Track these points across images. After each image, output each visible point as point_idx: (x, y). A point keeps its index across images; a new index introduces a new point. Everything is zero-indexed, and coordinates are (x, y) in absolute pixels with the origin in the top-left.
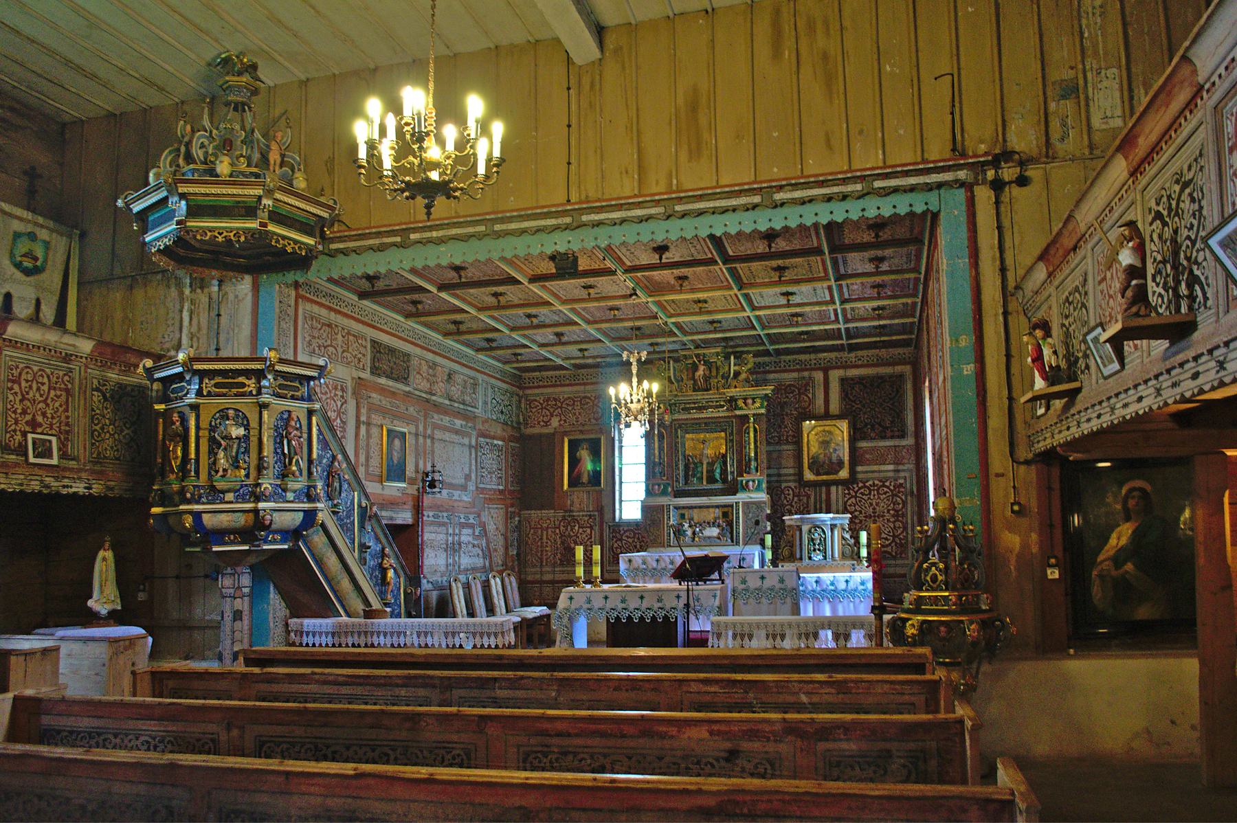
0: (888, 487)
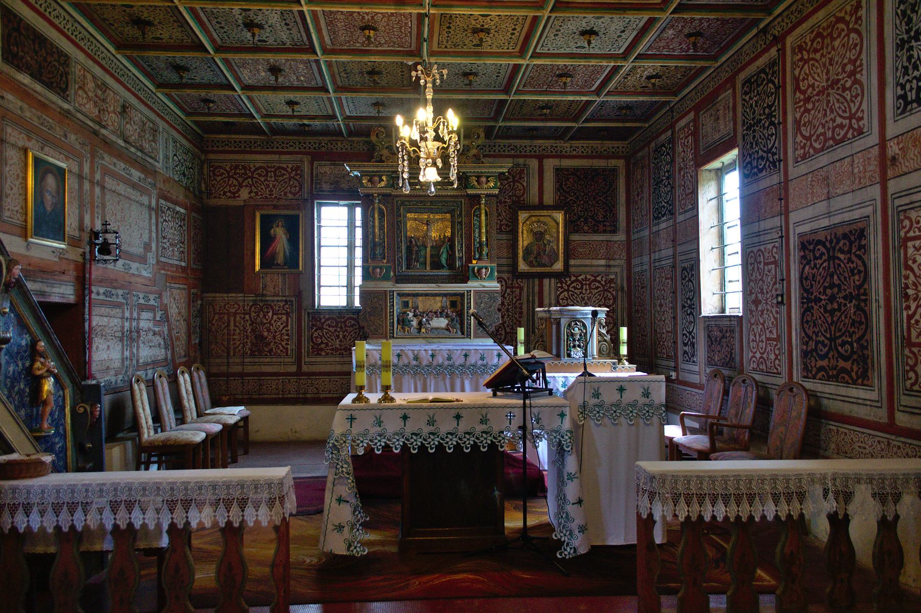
0: (599, 282)
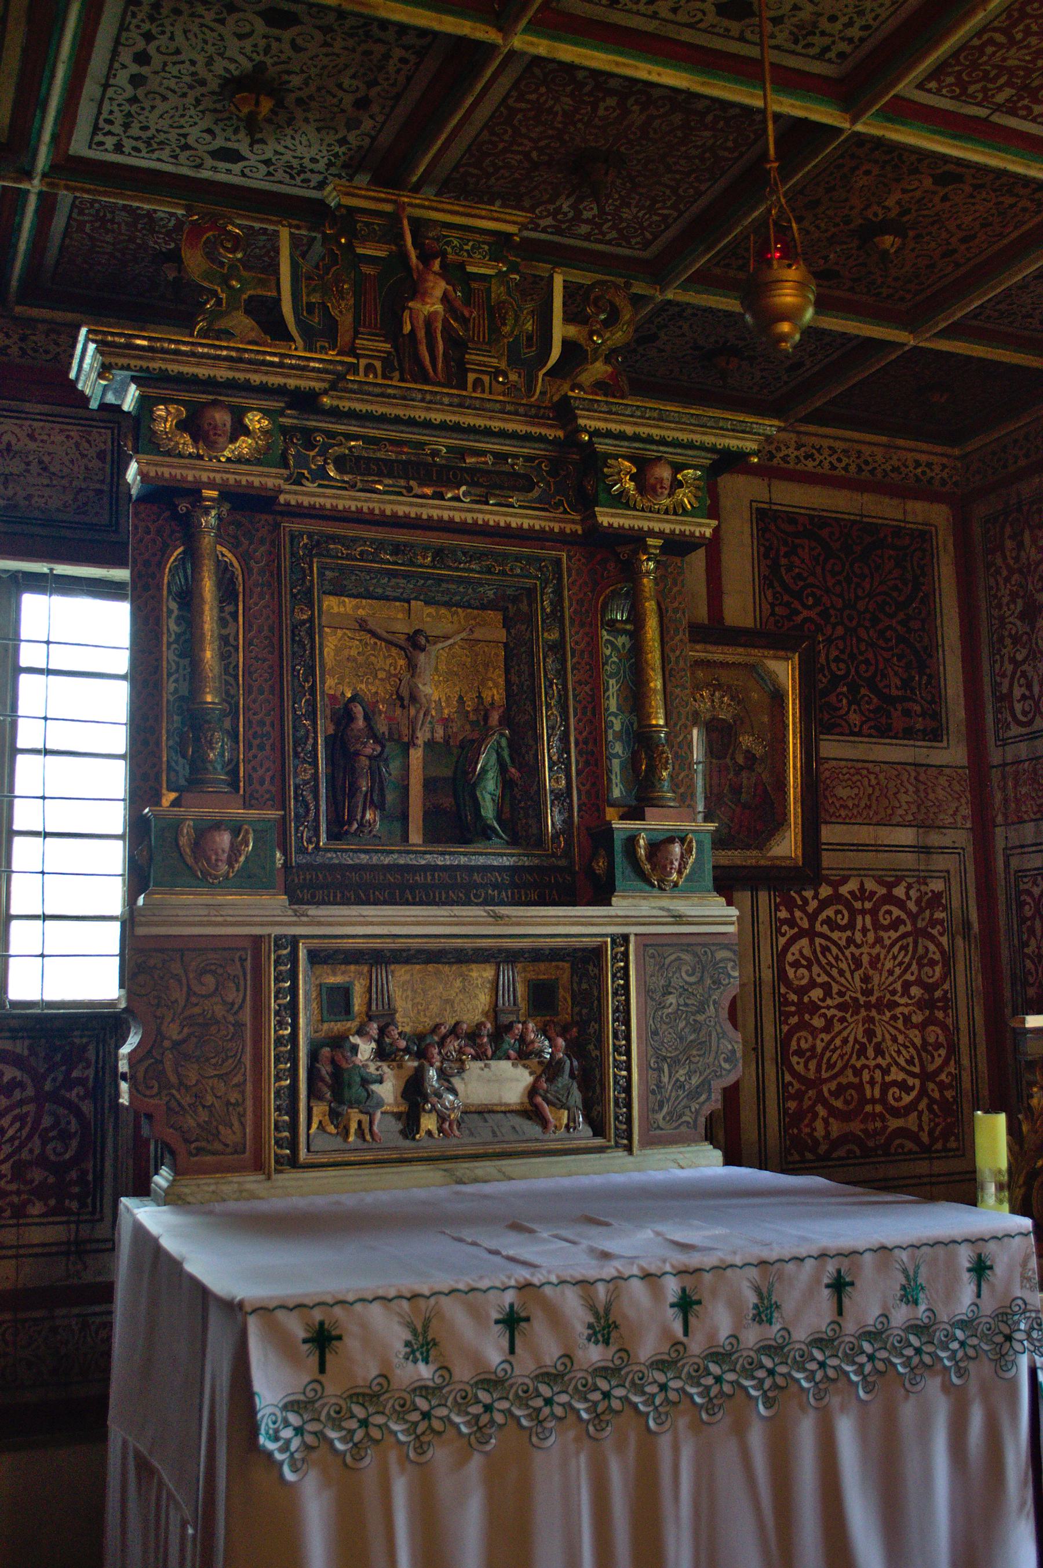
0: (901, 904)
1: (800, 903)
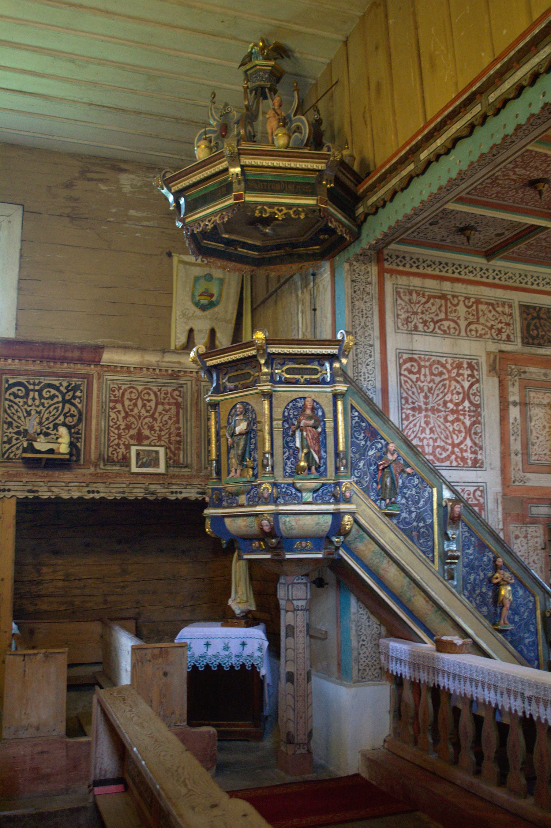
1: (459, 459)
